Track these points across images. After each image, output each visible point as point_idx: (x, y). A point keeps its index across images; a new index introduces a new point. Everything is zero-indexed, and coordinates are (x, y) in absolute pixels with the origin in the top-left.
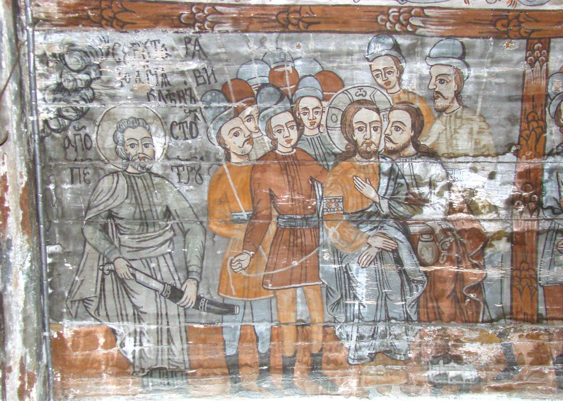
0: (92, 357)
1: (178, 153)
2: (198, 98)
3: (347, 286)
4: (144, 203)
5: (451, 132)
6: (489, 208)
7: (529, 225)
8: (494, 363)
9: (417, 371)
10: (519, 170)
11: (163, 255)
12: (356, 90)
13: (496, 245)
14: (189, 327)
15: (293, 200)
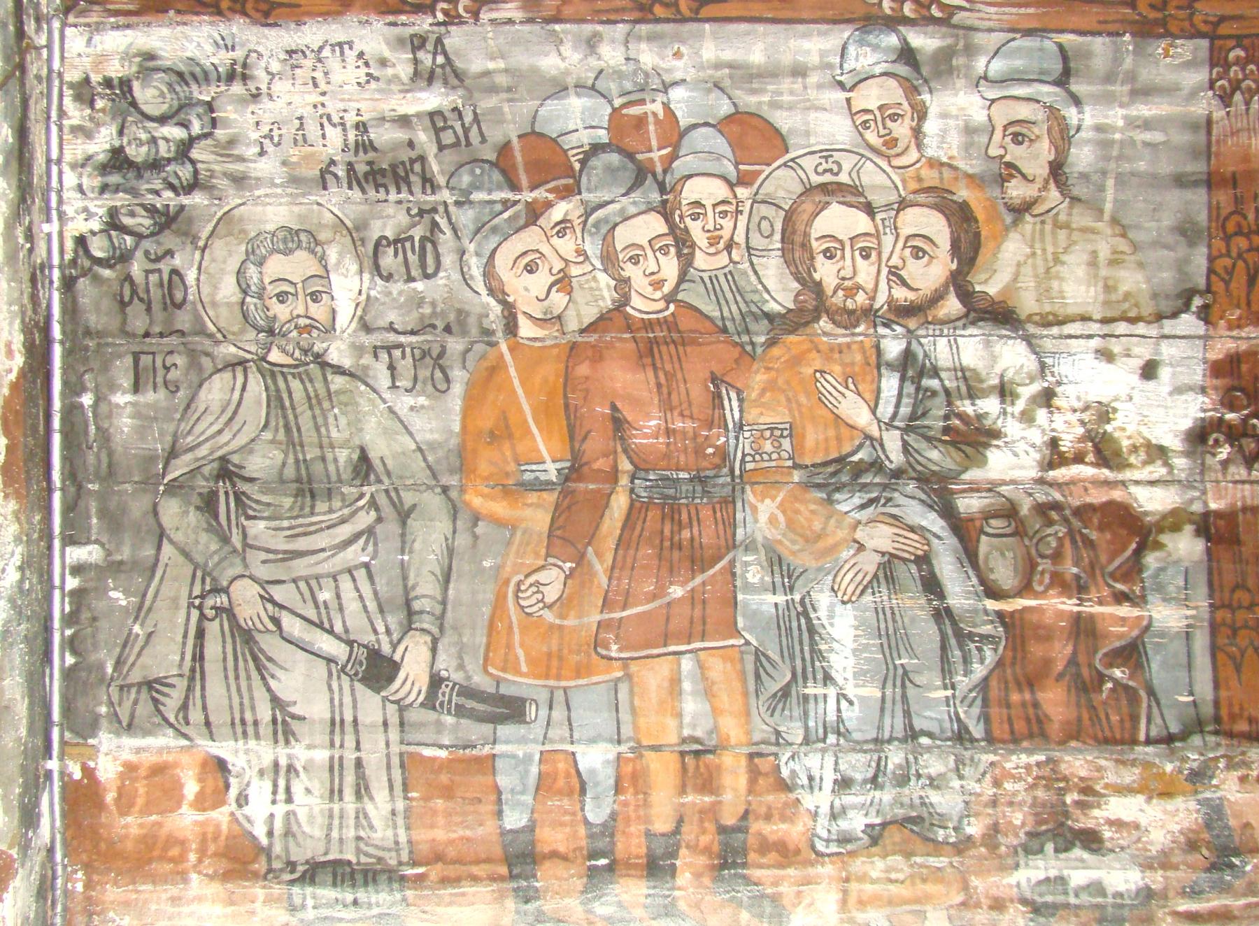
0: (164, 832)
1: (392, 316)
2: (441, 180)
3: (806, 648)
4: (306, 440)
5: (1046, 260)
6: (1147, 453)
7: (1247, 493)
8: (1184, 851)
9: (989, 871)
10: (1214, 355)
11: (350, 571)
12: (815, 159)
13: (1170, 546)
14: (411, 754)
15: (669, 432)
